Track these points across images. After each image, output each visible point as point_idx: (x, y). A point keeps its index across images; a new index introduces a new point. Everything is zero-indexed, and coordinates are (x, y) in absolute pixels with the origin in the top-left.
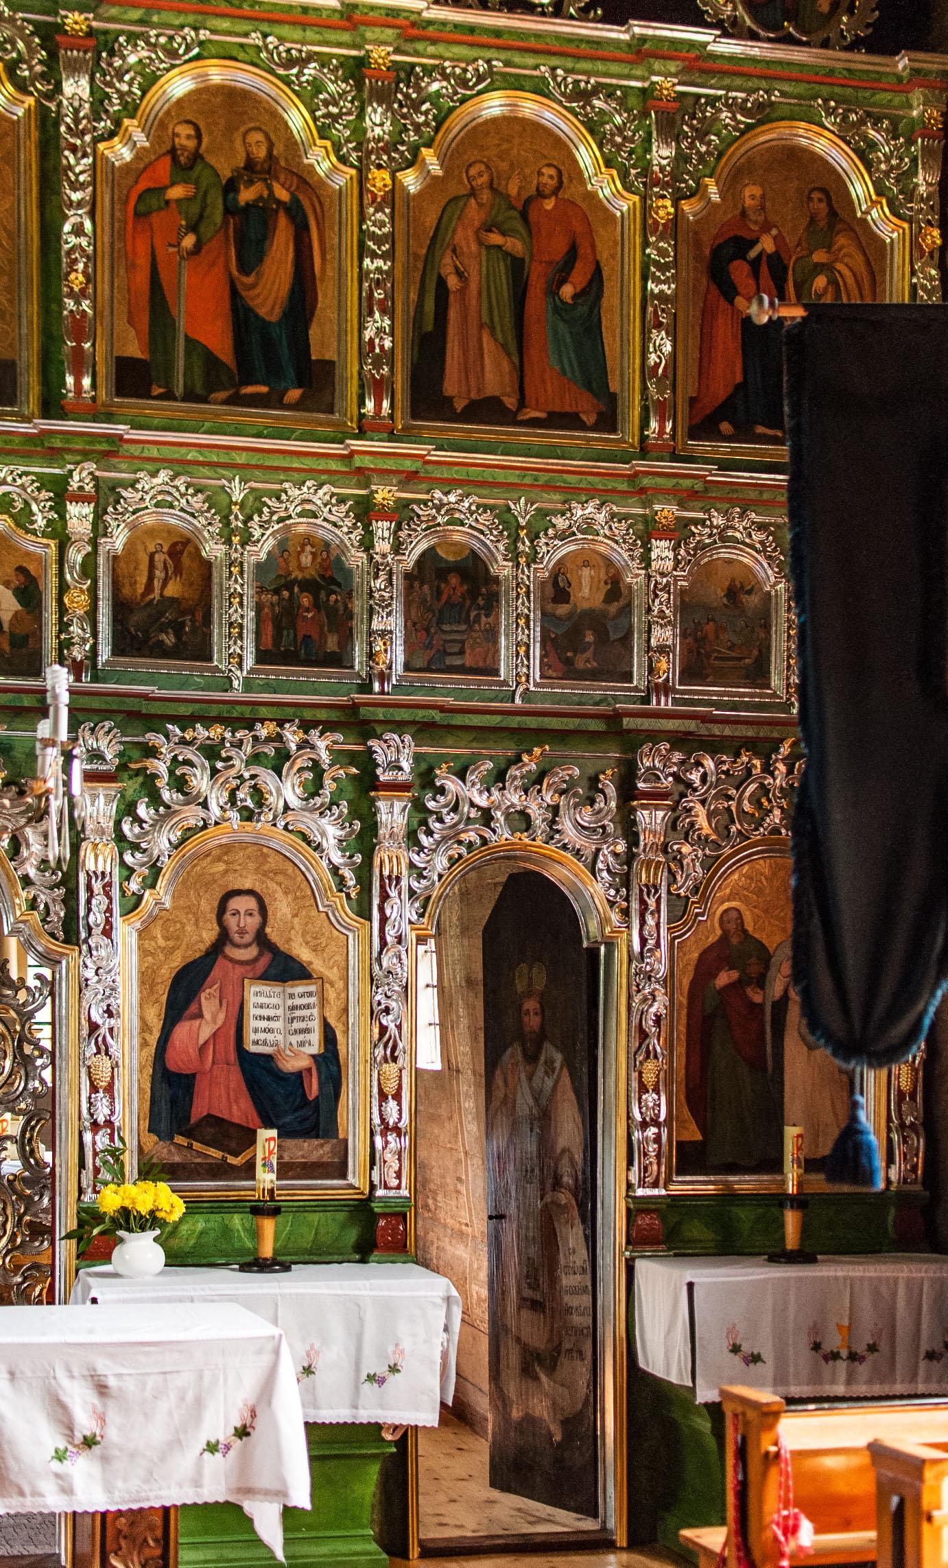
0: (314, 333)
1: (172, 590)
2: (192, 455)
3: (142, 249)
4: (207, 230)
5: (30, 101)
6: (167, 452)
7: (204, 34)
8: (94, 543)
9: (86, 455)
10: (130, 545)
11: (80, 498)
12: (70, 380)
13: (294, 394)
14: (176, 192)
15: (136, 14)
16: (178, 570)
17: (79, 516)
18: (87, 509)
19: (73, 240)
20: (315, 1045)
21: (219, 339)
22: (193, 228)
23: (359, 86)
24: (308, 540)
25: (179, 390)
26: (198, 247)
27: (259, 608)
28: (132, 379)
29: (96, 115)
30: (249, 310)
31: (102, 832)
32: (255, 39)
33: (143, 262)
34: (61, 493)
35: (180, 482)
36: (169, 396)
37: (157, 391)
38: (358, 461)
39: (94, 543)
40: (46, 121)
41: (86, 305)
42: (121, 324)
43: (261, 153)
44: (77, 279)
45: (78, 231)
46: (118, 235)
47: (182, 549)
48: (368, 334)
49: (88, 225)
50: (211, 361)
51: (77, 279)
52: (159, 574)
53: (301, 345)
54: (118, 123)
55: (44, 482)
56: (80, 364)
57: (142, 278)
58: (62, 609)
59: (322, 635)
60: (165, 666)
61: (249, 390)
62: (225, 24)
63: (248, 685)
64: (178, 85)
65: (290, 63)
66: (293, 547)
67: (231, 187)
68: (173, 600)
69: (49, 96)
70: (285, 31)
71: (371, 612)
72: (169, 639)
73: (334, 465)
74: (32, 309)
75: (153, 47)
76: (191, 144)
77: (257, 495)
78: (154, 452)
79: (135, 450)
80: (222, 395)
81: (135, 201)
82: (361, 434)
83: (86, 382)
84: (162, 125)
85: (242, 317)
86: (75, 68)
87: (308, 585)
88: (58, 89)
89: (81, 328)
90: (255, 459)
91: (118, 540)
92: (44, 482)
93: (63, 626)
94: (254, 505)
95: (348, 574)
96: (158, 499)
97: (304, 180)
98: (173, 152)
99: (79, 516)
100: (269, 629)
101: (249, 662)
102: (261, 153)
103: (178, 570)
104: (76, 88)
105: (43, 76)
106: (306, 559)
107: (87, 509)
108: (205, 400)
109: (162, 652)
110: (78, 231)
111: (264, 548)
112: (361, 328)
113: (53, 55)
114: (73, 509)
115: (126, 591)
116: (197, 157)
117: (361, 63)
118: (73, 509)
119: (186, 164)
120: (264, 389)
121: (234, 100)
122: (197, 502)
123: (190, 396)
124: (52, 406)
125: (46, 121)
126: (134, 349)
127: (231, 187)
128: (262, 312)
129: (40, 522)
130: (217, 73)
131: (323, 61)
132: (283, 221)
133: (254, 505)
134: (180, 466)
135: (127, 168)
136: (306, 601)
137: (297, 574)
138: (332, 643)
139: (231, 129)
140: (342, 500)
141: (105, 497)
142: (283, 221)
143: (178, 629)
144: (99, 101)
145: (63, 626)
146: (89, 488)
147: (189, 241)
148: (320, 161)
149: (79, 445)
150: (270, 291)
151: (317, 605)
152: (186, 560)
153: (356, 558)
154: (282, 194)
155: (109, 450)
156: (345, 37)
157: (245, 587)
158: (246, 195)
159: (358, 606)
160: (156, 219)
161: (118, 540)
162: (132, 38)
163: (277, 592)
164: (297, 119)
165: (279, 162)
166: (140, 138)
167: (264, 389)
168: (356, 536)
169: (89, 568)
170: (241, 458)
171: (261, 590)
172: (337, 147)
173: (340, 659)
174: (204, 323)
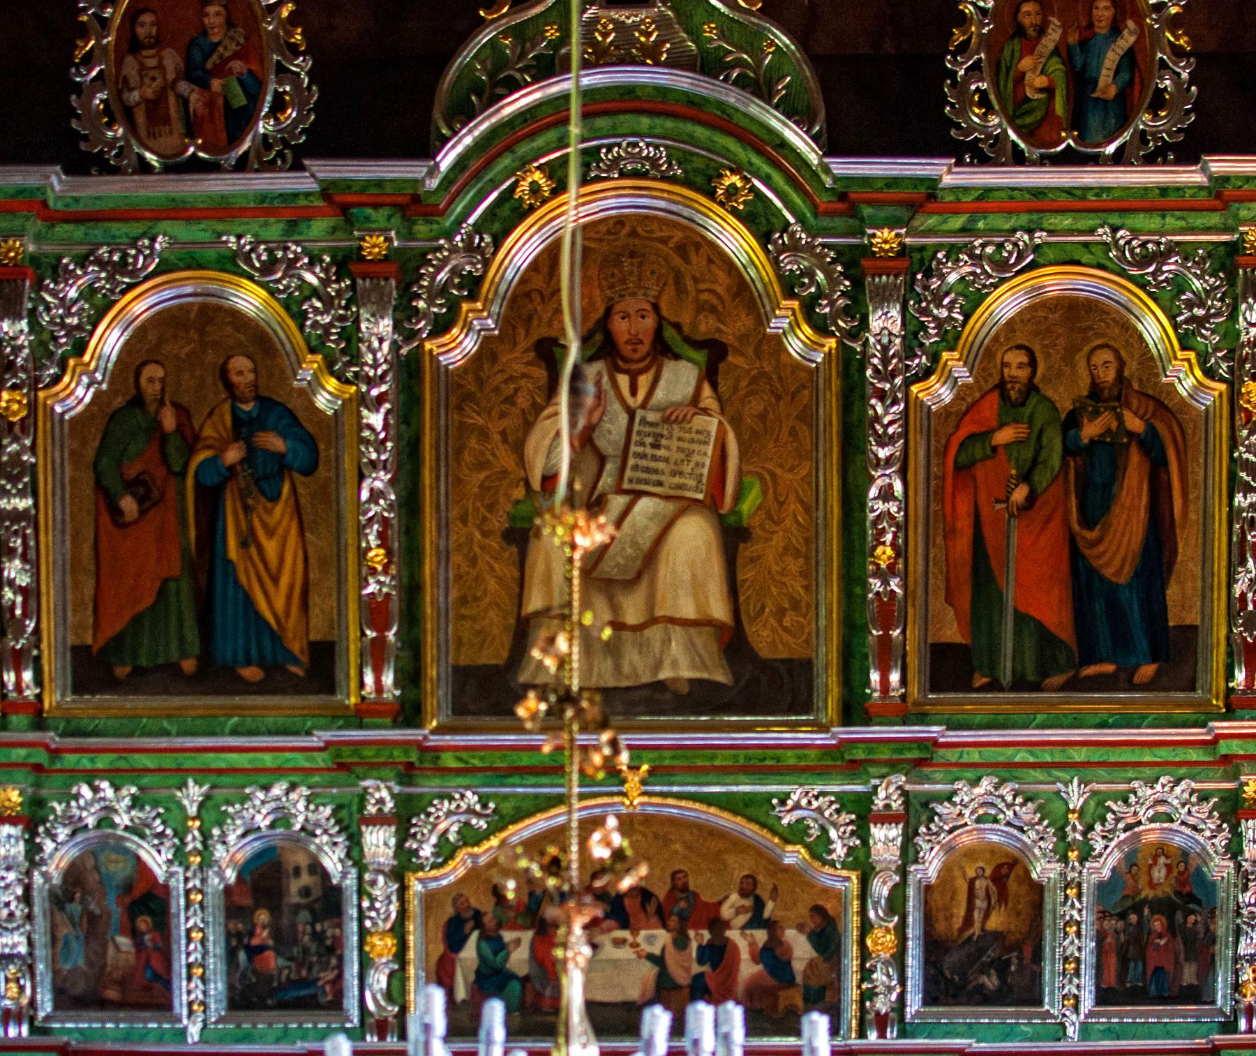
0: (1173, 593)
1: (996, 922)
2: (1021, 756)
3: (964, 507)
4: (1042, 478)
5: (832, 343)
6: (990, 755)
7: (1040, 238)
8: (903, 872)
9: (894, 766)
10: (946, 871)
11: (887, 818)
12: (875, 677)
13: (1147, 671)
14: (1005, 436)
15: (957, 222)
16: (1003, 897)
17: (885, 837)
18: (895, 832)
19: (880, 506)
20: (648, 964)
21: (1055, 613)
22: (1026, 477)
23: (1231, 279)
24: (1161, 849)
25: (1007, 677)
26: (1031, 499)
27: (1100, 937)
28: (950, 669)
29: (909, 351)
30: (1093, 573)
31: (876, 904)
32: (1103, 234)
33: (964, 524)
34: (864, 815)
35: (1006, 791)
36: (994, 686)
37: (980, 681)
38: (1224, 748)
39: (903, 872)
40: (850, 365)
41: (894, 585)
42: (938, 602)
43: (1109, 376)
44: (885, 553)
45: (887, 494)
46: (936, 493)
47: (1007, 871)
48: (1238, 589)
49: (898, 487)
50: (1045, 638)
51: (885, 553)
52: (980, 903)
53: (1155, 608)
54: (935, 358)
55: (844, 803)
56: (887, 655)
57: (963, 544)
58: (864, 954)
59: (1178, 965)
60: (986, 1016)
61: (1091, 670)
62: (1066, 221)
63: (1085, 1031)
64: (1006, 303)
65: (1144, 260)
66: (1143, 859)
67: (1072, 422)
68: (998, 935)
69: (853, 335)
70: (1139, 221)
71: (1238, 932)
72: (990, 982)
73: (1194, 755)
74: (831, 595)
75: (977, 259)
76: (1023, 374)
77: (1099, 799)
78: (974, 756)
79: (952, 755)
80: (1058, 680)
81: (955, 452)
82: (1230, 712)
83: (895, 677)
84: (989, 354)
85: (1083, 579)
86: (883, 297)
87: (1164, 907)
88: (864, 324)
89: (889, 611)
90: (1097, 755)
91: (931, 865)
92: (844, 803)
93: (866, 974)
94: (1095, 814)
95: (1210, 887)
96: (977, 813)
97: (1163, 405)
98: (1001, 386)
99: (885, 837)
100: (1113, 962)
101: (1087, 1003)
102: (1109, 376)
103: (1003, 897)
104: (885, 321)
105: (847, 312)
106: (1159, 874)
107: (895, 832)
108: (1036, 687)
109: (984, 998)
110: (887, 494)
111: (1106, 864)
112: (1231, 581)
113: (858, 284)
114: (879, 833)
115: (941, 927)
116: (1031, 388)
117: (1234, 249)
118: (879, 833)
119: (1013, 398)
120: (1109, 668)
121: (1076, 314)
122: (1027, 812)
123: (1020, 684)
124: (854, 709)
125: (850, 365)
126: (952, 633)
127: (1072, 422)
128: (1108, 572)
129: (840, 851)
130: (1055, 282)
131: (1186, 252)
132: (1135, 457)
133: (1095, 814)
134: (1006, 770)
135: (946, 411)
136: (1157, 924)
137: (1147, 893)
138: (1189, 975)
139: (1072, 351)
140: (1204, 797)
141: (915, 815)
142: (1135, 457)
143: (1002, 968)
144: (912, 333)
145: (866, 974)
146: (896, 805)
147: (1020, 494)
148: (1184, 379)
149: (885, 754)
150: (1118, 547)
151: (1171, 930)
152: (1012, 885)
153: (1220, 868)
154: (1134, 424)
155: (921, 759)
156: (1214, 219)
157: (1082, 912)
158: (1090, 430)
159: (1222, 927)
160: (980, 472)
161: (931, 865)
162: (953, 251)
163: (1122, 916)
164: (1153, 328)
165: (1136, 382)
166: (961, 372)
167: (1109, 668)
168: (1221, 841)
169: (896, 904)
170: (1080, 755)
171: (1103, 915)
172: (1203, 358)
173: (1198, 994)
174: (1035, 591)
